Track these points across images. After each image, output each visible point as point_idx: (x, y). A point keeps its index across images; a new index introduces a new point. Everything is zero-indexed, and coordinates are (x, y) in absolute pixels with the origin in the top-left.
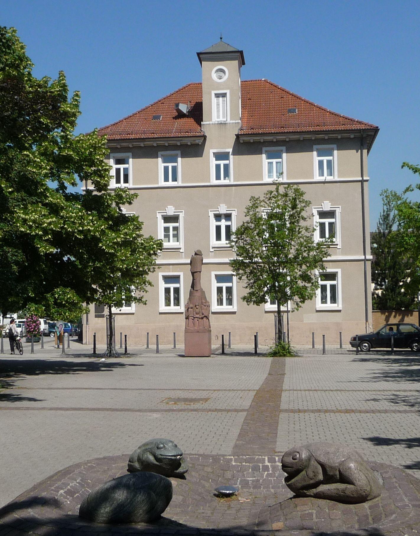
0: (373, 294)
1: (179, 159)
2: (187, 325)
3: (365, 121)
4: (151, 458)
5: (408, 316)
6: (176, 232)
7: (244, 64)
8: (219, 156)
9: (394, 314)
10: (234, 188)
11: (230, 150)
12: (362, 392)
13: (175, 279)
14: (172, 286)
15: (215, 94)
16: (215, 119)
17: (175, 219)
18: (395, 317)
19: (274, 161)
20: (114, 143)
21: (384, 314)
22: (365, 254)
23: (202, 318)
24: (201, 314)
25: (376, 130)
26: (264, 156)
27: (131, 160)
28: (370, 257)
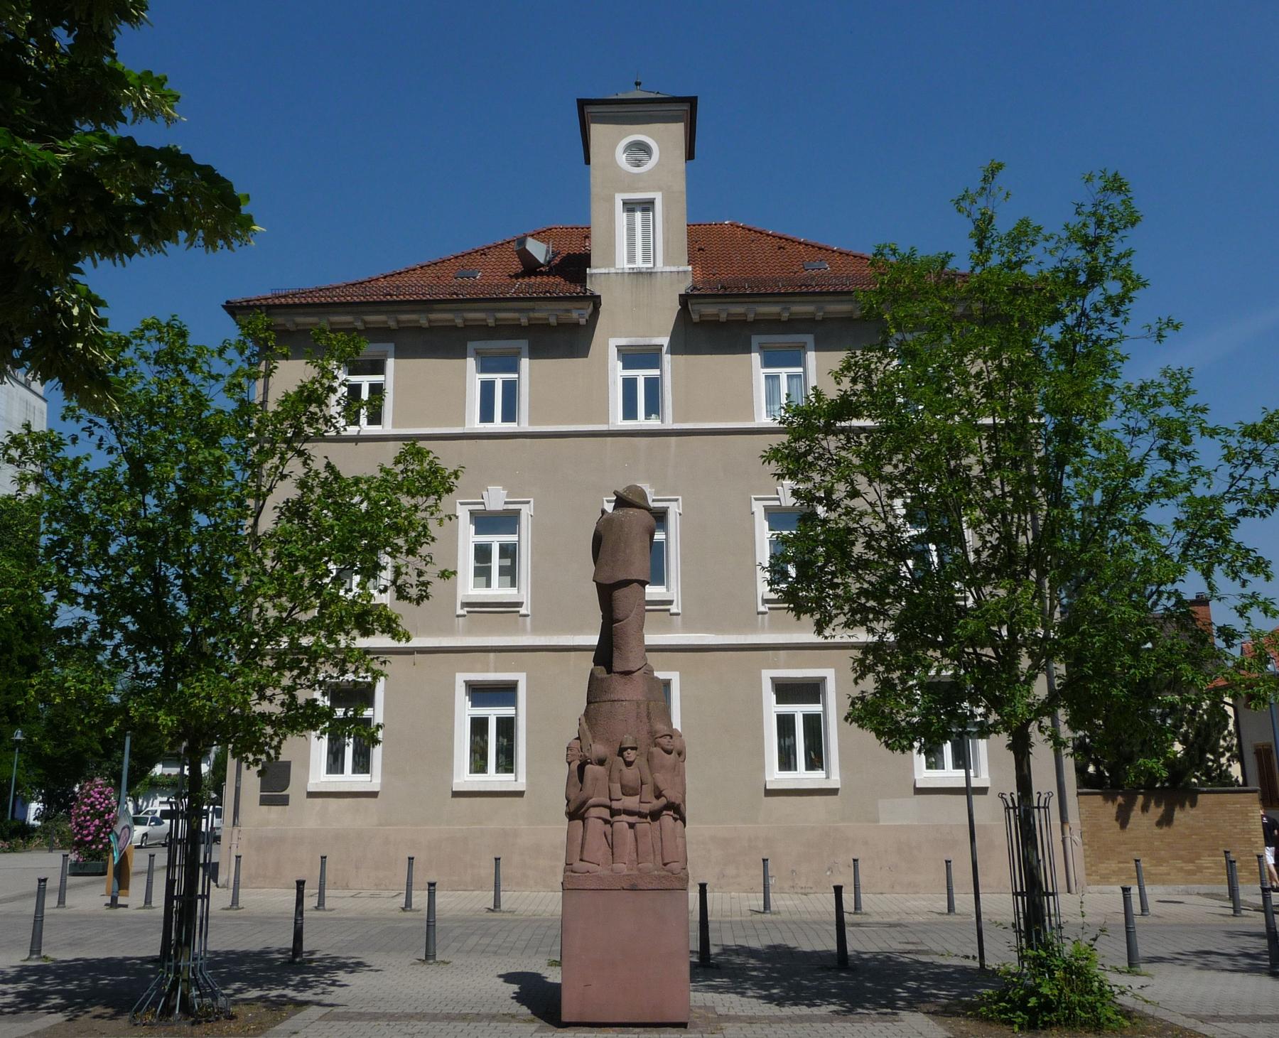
1: (525, 363)
2: (577, 851)
5: (1182, 806)
6: (507, 562)
8: (632, 357)
9: (1140, 799)
10: (673, 439)
11: (664, 341)
15: (625, 203)
16: (622, 263)
17: (506, 521)
18: (1145, 808)
19: (783, 372)
20: (348, 313)
21: (1114, 800)
23: (655, 815)
24: (647, 791)
26: (756, 358)
27: (390, 363)
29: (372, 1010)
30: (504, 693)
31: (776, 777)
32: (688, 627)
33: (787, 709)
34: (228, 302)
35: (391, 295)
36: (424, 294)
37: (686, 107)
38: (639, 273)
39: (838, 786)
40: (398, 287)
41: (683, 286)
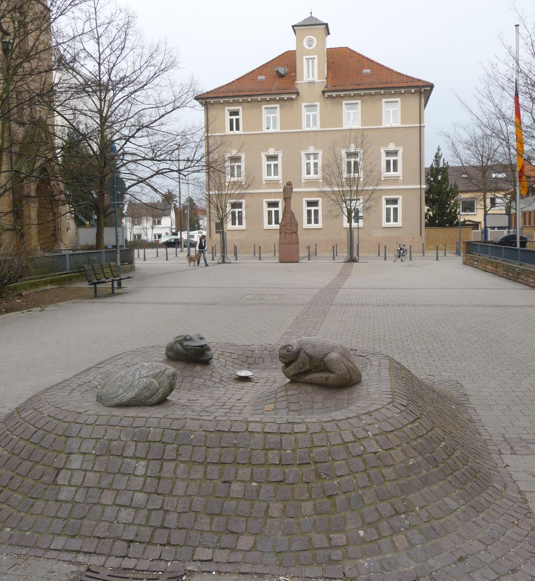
0: (426, 214)
2: (281, 238)
3: (424, 79)
4: (180, 347)
7: (329, 34)
12: (399, 290)
13: (275, 204)
14: (313, 209)
16: (306, 79)
17: (273, 158)
22: (421, 185)
25: (432, 86)
28: (424, 186)
33: (309, 208)
37: (324, 26)
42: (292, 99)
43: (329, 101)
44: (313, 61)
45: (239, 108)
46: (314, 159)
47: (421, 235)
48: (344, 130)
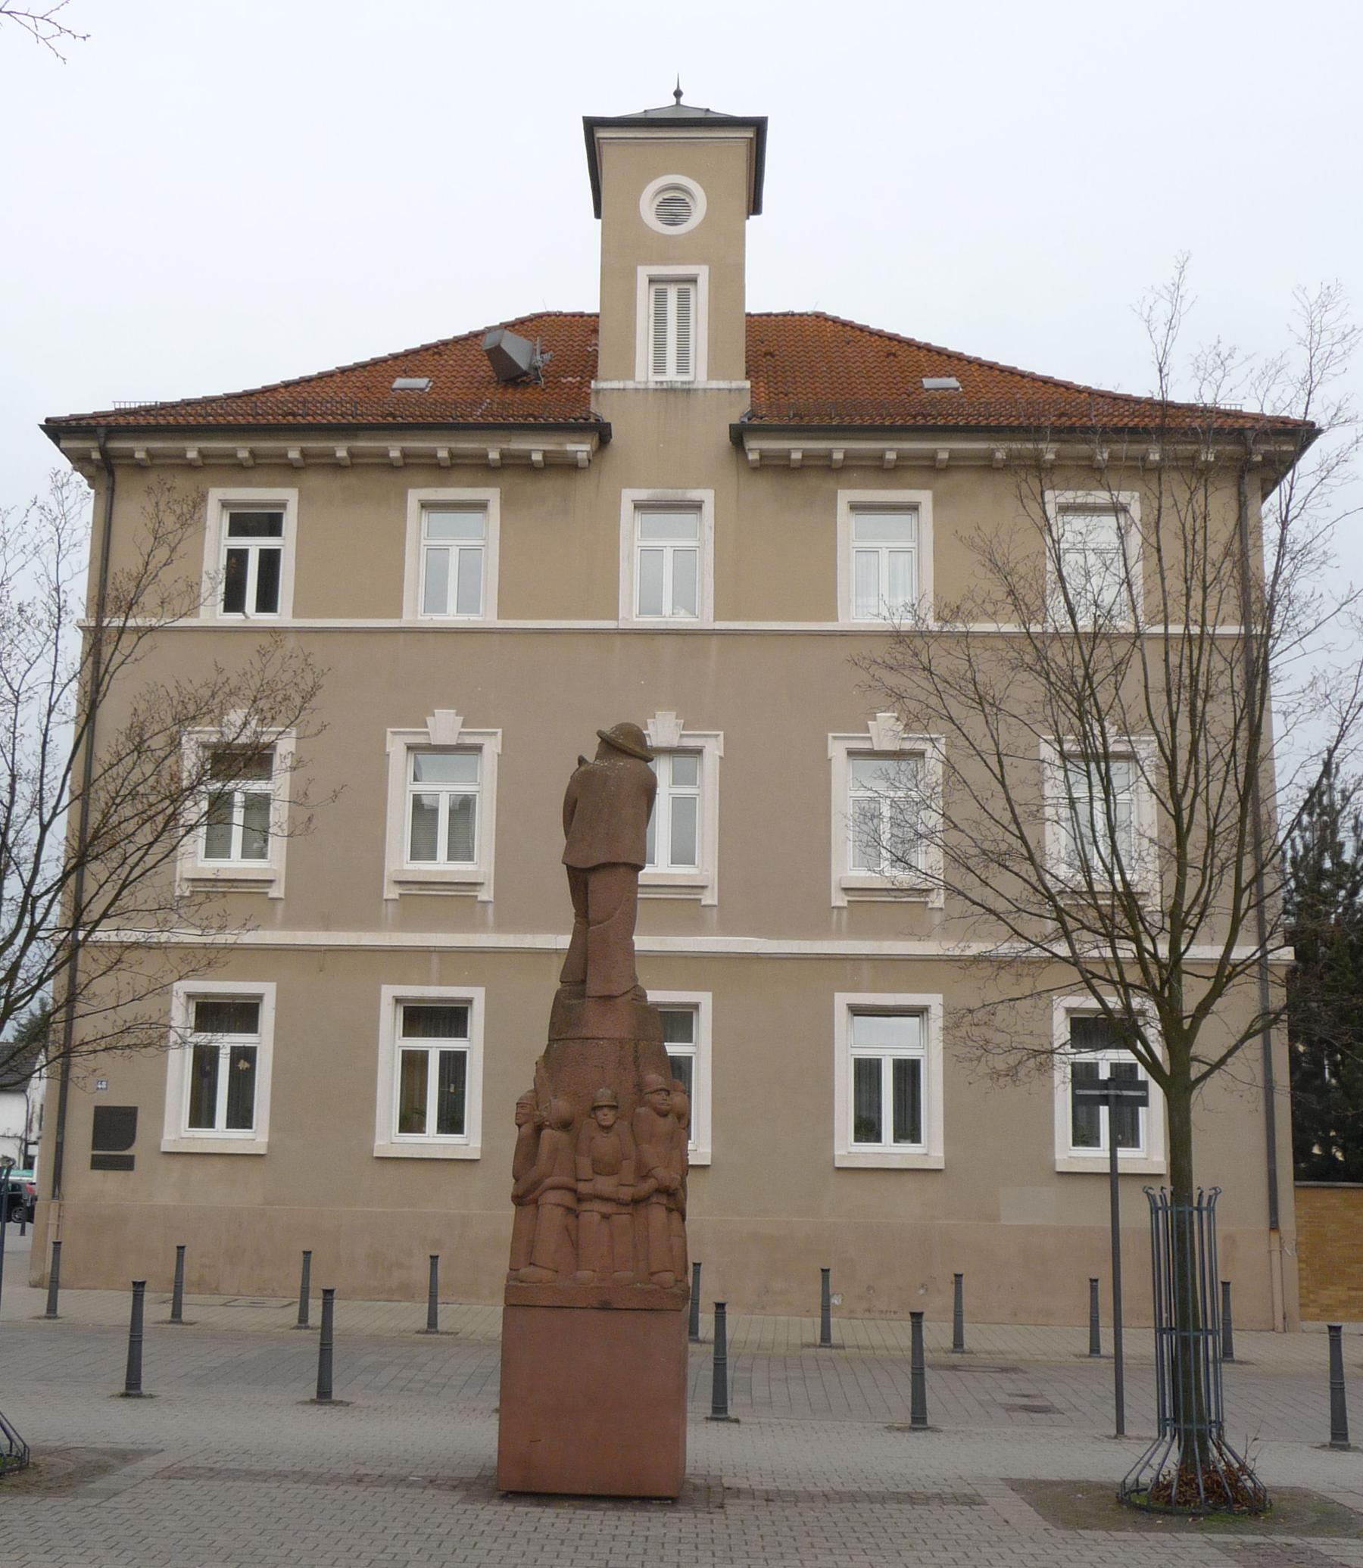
14: (434, 1046)
16: (644, 374)
29: (231, 1466)
30: (448, 1018)
31: (848, 1149)
32: (728, 928)
34: (47, 420)
35: (294, 415)
36: (235, 414)
37: (750, 134)
38: (669, 391)
39: (941, 1166)
40: (304, 402)
41: (736, 412)
42: (569, 467)
43: (763, 487)
44: (683, 296)
45: (288, 496)
46: (676, 781)
47: (1274, 1226)
48: (844, 634)
